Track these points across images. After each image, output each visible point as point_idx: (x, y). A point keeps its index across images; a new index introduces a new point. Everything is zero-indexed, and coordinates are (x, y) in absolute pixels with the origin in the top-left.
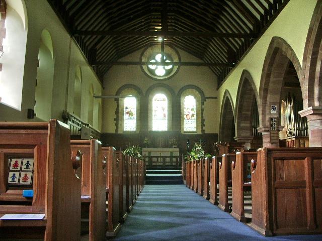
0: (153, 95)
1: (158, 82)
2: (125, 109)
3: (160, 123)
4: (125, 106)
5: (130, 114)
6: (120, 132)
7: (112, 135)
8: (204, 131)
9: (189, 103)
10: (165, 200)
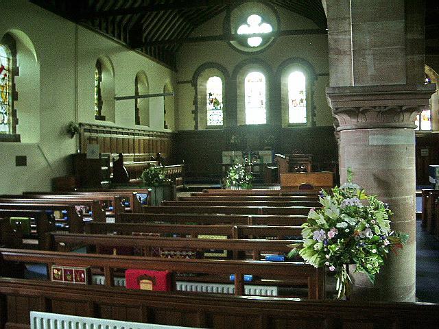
0: (244, 75)
1: (247, 57)
2: (208, 97)
3: (255, 113)
4: (208, 92)
5: (216, 103)
6: (200, 129)
7: (189, 133)
8: (315, 122)
9: (296, 82)
10: (36, 203)
